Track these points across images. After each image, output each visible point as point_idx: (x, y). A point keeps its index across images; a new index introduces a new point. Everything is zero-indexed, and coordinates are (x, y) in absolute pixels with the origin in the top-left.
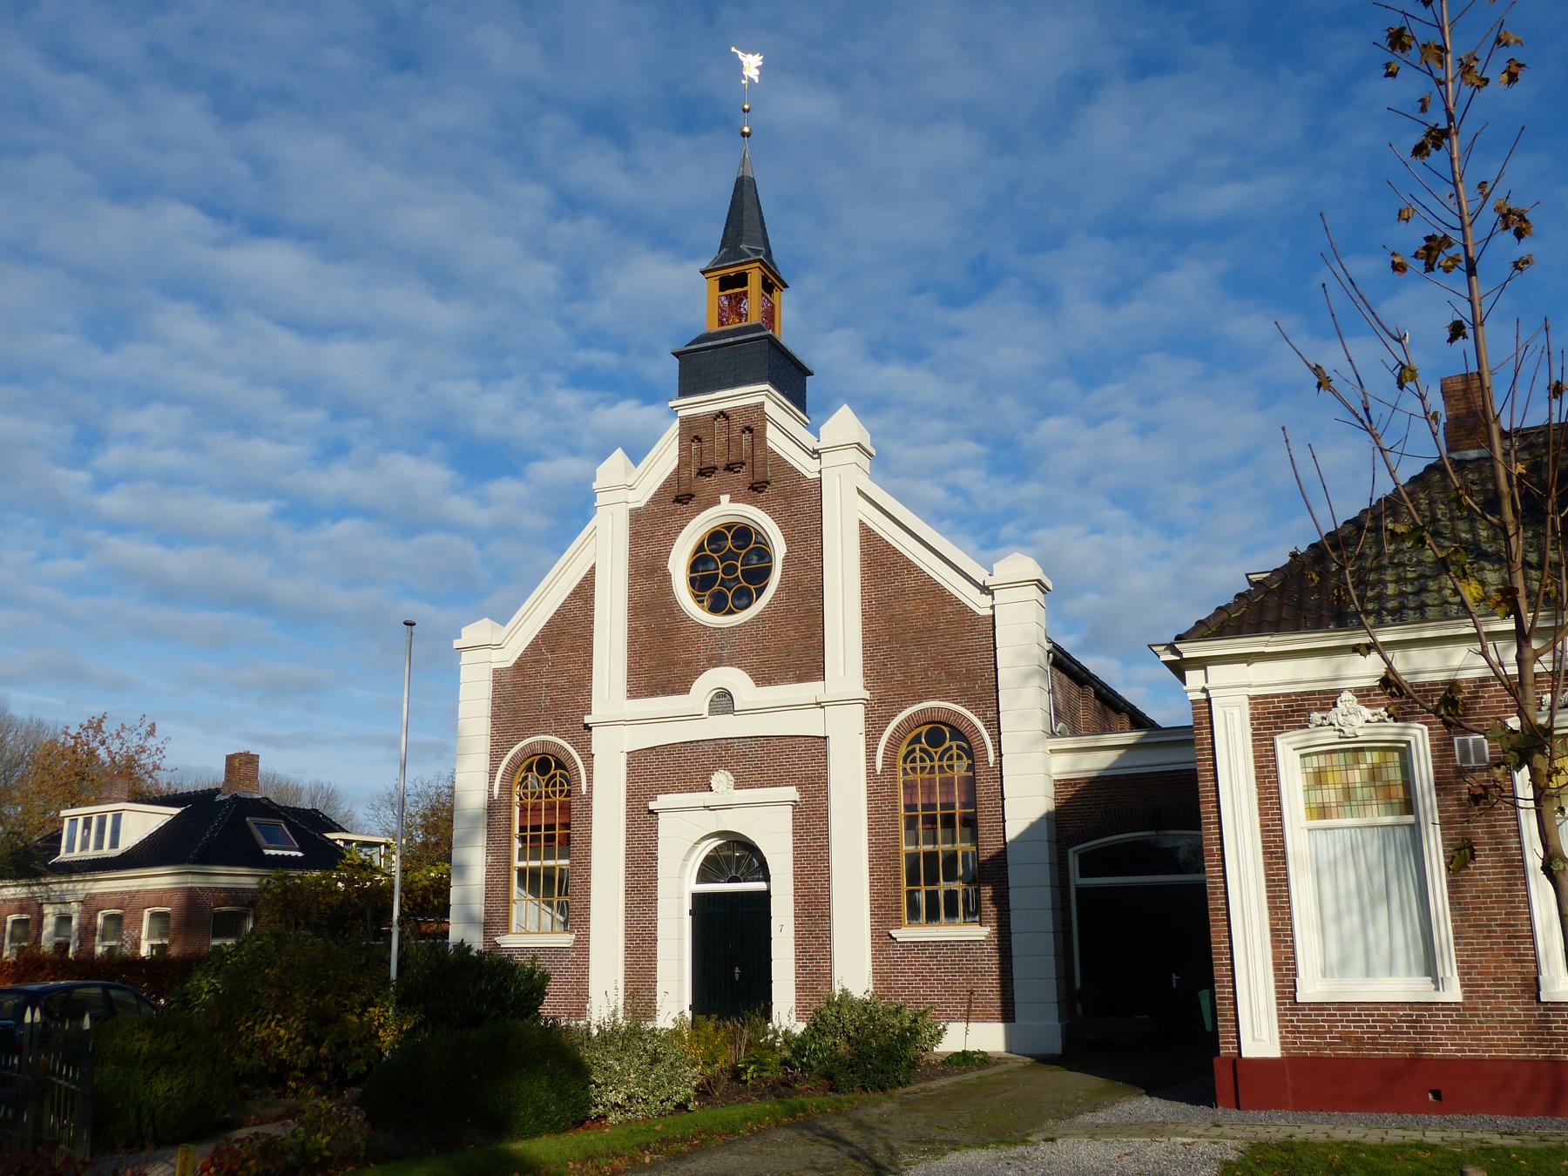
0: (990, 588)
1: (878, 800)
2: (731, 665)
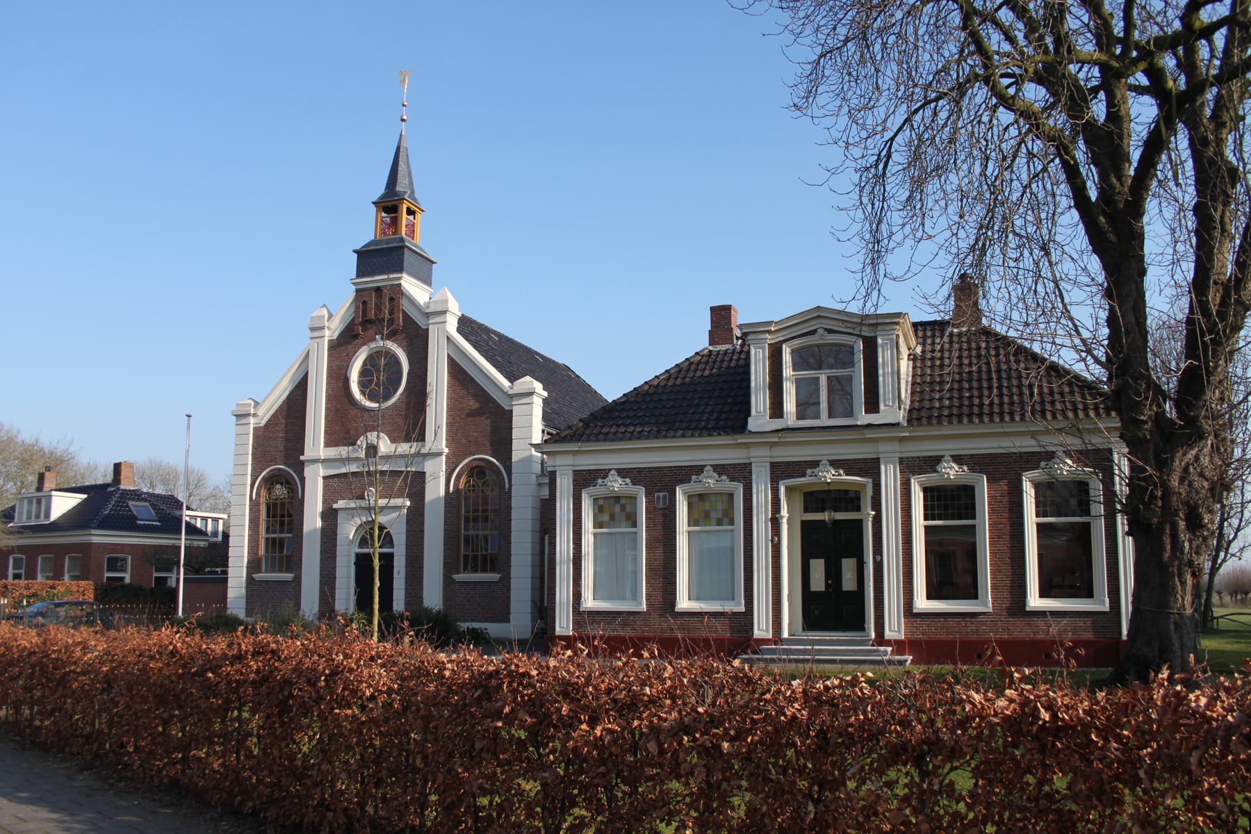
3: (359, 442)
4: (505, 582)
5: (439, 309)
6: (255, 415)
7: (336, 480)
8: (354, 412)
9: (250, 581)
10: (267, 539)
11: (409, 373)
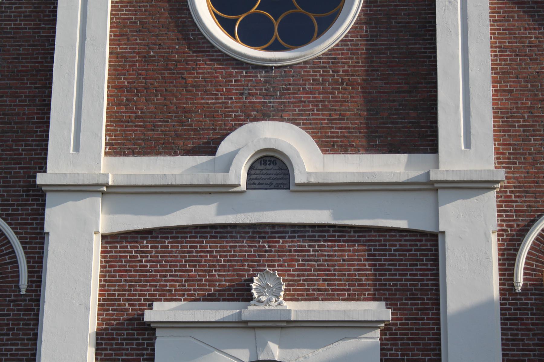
0: (152, 325)
1: (517, 330)
2: (282, 119)
3: (224, 148)
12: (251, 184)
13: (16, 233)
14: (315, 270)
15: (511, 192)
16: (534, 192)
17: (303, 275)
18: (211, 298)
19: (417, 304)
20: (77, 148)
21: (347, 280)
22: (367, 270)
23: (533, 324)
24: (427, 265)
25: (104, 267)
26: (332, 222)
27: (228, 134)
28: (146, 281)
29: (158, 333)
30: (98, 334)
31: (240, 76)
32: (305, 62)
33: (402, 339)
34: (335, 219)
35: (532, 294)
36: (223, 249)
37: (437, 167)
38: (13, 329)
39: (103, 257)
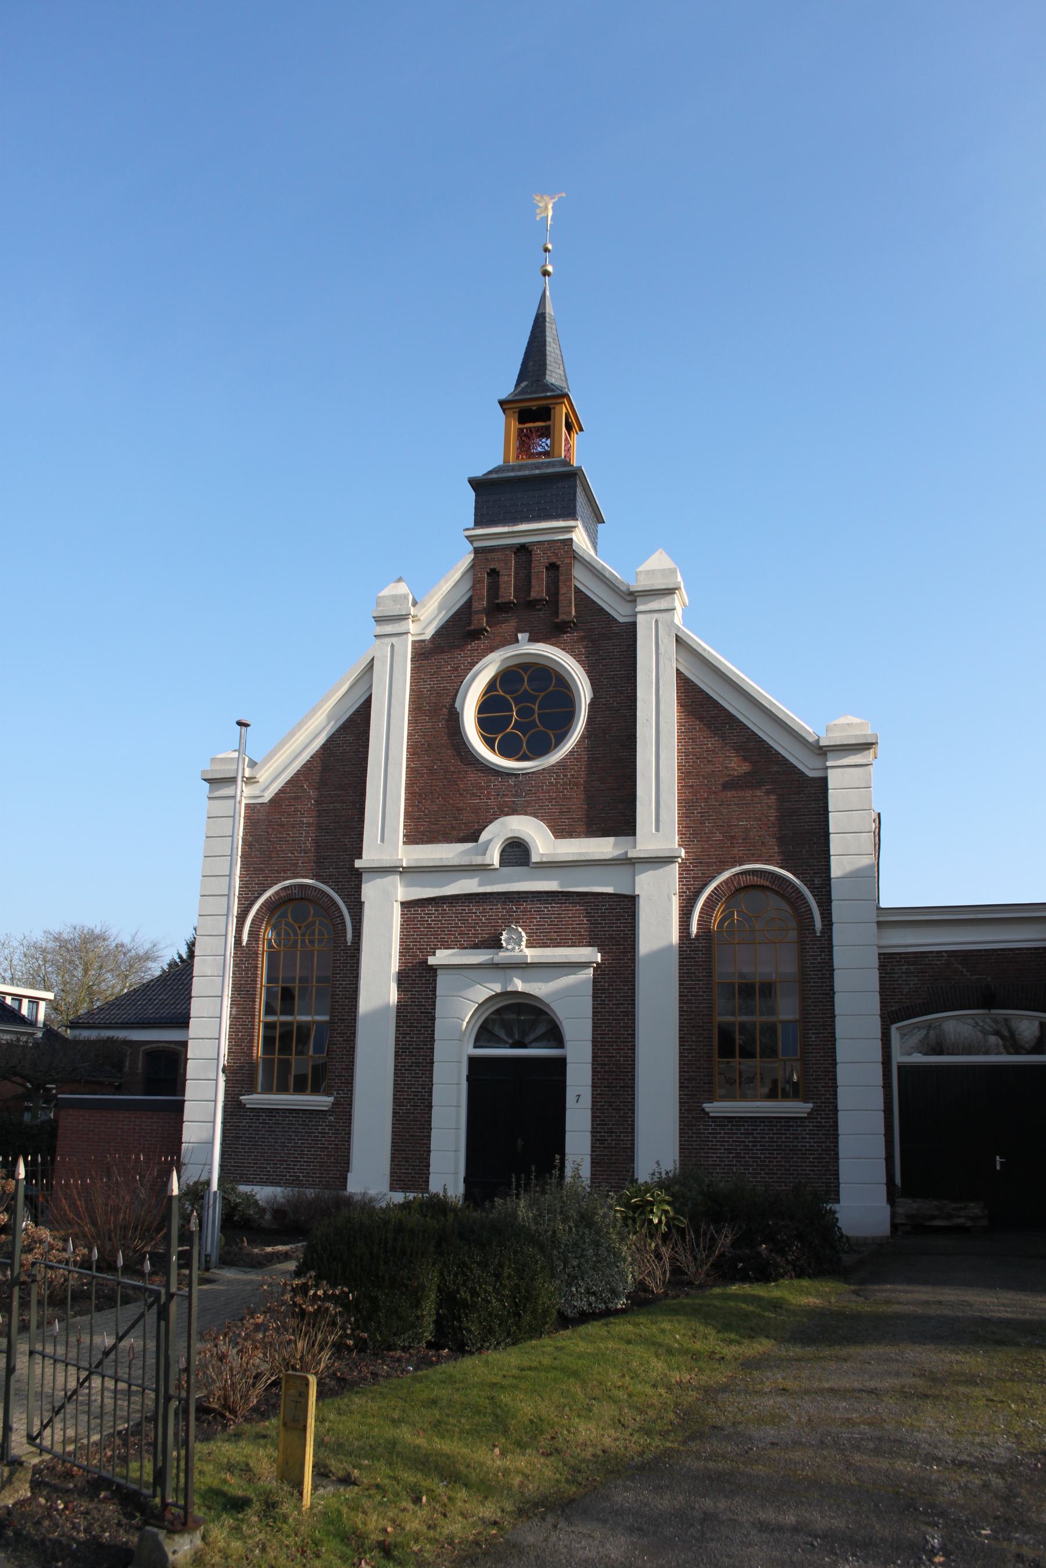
2: (526, 814)
3: (484, 836)
4: (343, 1110)
5: (659, 584)
6: (250, 781)
7: (432, 909)
8: (473, 776)
9: (233, 1109)
10: (268, 1026)
11: (592, 705)
12: (503, 863)
13: (344, 902)
14: (549, 925)
15: (690, 863)
16: (706, 863)
17: (540, 929)
18: (476, 946)
19: (620, 949)
20: (382, 840)
21: (571, 932)
22: (585, 924)
23: (703, 961)
24: (627, 919)
25: (683, 910)
26: (560, 890)
27: (487, 826)
28: (432, 935)
29: (439, 972)
30: (399, 973)
31: (497, 781)
32: (543, 769)
33: (609, 974)
34: (561, 887)
35: (703, 939)
36: (484, 911)
37: (635, 847)
38: (343, 970)
39: (402, 918)
